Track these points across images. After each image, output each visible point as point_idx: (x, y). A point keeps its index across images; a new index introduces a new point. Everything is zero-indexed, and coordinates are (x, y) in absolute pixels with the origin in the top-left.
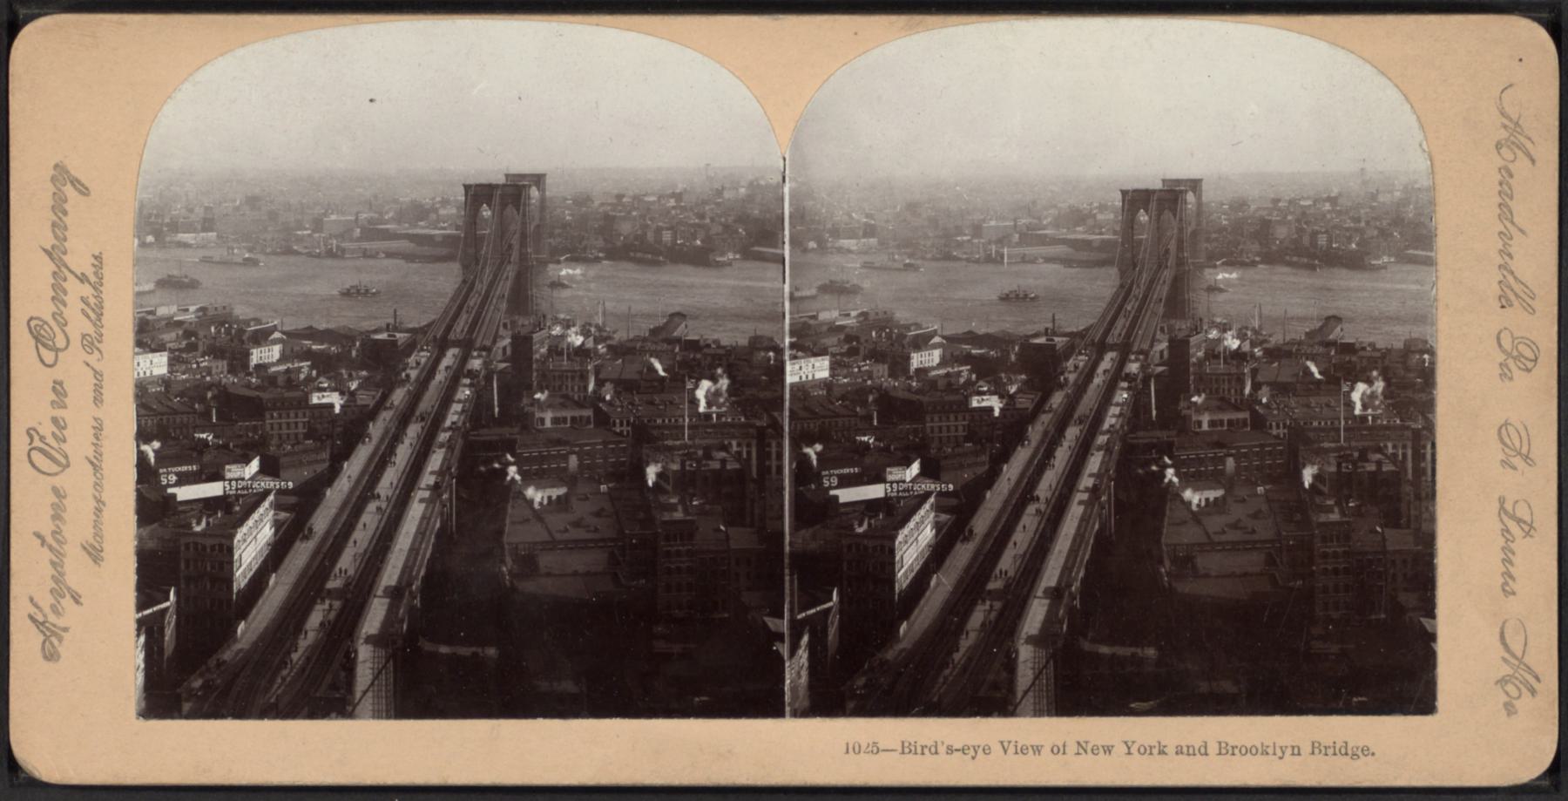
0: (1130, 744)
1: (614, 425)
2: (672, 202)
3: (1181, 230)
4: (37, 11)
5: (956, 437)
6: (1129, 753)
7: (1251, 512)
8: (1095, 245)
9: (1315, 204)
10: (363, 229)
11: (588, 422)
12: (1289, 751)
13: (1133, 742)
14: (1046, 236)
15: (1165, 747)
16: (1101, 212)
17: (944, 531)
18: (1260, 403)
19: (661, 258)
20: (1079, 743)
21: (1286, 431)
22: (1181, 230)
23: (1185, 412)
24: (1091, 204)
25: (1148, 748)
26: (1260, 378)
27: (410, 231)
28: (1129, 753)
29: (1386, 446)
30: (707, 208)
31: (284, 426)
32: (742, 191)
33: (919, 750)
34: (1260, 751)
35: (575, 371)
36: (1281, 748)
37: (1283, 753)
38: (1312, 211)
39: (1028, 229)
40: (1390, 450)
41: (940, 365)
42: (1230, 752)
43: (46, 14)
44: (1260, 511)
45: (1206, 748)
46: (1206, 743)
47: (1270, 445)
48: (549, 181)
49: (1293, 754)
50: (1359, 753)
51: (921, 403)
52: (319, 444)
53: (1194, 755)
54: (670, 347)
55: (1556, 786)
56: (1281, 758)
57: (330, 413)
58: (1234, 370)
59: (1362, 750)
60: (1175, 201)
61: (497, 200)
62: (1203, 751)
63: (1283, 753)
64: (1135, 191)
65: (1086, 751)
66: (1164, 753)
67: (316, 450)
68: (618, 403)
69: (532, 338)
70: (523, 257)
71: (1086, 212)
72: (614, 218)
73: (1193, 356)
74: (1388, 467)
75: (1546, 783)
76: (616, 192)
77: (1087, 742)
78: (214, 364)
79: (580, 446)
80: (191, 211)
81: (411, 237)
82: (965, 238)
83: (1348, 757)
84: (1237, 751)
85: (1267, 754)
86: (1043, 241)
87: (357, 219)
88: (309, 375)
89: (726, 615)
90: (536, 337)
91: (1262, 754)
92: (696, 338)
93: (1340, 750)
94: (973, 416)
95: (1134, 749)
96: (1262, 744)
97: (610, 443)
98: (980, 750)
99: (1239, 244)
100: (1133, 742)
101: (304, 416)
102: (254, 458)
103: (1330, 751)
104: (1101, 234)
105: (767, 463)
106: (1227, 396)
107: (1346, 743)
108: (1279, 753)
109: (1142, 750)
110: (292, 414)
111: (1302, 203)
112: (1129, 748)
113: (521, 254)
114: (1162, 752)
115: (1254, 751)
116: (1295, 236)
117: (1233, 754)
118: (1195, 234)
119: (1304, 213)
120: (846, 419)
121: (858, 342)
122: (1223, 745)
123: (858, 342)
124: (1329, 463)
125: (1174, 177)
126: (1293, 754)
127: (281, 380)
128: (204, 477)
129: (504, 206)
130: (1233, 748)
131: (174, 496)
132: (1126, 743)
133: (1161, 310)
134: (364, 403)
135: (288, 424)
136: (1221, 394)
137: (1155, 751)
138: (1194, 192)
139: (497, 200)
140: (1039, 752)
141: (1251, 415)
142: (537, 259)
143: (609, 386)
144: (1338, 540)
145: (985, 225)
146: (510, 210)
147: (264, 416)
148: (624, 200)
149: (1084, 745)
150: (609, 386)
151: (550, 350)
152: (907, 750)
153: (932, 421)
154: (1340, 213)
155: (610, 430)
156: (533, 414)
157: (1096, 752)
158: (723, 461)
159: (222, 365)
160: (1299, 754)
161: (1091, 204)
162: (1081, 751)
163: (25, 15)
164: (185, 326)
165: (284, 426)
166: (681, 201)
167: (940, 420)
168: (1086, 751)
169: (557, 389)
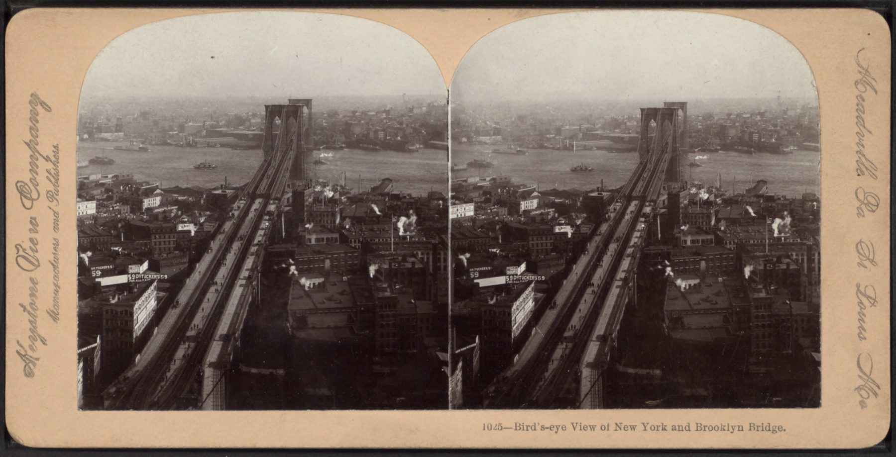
0: (646, 424)
2: (384, 115)
4: (21, 6)
5: (546, 249)
6: (645, 430)
9: (751, 117)
12: (736, 429)
13: (648, 423)
15: (666, 426)
18: (720, 230)
19: (378, 147)
20: (616, 424)
21: (735, 246)
23: (677, 235)
25: (656, 427)
26: (720, 216)
27: (235, 132)
28: (645, 430)
31: (162, 243)
32: (424, 109)
33: (525, 428)
34: (720, 429)
36: (732, 427)
37: (733, 430)
38: (750, 120)
42: (703, 429)
43: (26, 8)
45: (689, 427)
46: (689, 424)
47: (725, 254)
49: (739, 430)
50: (777, 429)
51: (526, 230)
52: (182, 253)
53: (683, 430)
55: (889, 449)
56: (732, 433)
59: (779, 428)
60: (672, 115)
61: (284, 114)
62: (687, 428)
63: (733, 430)
64: (648, 109)
65: (620, 429)
66: (665, 430)
68: (353, 230)
70: (299, 147)
71: (620, 121)
75: (883, 447)
76: (352, 109)
77: (621, 424)
79: (332, 254)
81: (235, 136)
83: (771, 432)
84: (707, 429)
85: (724, 430)
88: (177, 214)
91: (721, 430)
92: (398, 193)
93: (685, 428)
95: (648, 428)
96: (721, 424)
98: (560, 429)
99: (708, 139)
100: (648, 423)
102: (145, 261)
103: (760, 429)
105: (438, 264)
107: (769, 424)
108: (731, 430)
109: (653, 428)
112: (645, 427)
113: (298, 145)
114: (664, 429)
115: (716, 428)
116: (740, 135)
117: (705, 430)
118: (683, 133)
120: (105, 238)
122: (699, 425)
124: (759, 264)
126: (739, 430)
127: (160, 217)
129: (288, 118)
130: (705, 426)
131: (100, 283)
132: (643, 424)
135: (165, 242)
136: (698, 225)
137: (660, 429)
138: (683, 110)
139: (284, 114)
140: (594, 429)
142: (307, 148)
143: (348, 220)
146: (292, 120)
147: (151, 237)
149: (619, 425)
151: (314, 200)
152: (518, 428)
153: (533, 240)
155: (349, 245)
157: (626, 429)
159: (127, 208)
160: (742, 430)
161: (624, 116)
162: (618, 428)
163: (14, 8)
165: (162, 243)
167: (537, 240)
168: (620, 429)
169: (694, 223)
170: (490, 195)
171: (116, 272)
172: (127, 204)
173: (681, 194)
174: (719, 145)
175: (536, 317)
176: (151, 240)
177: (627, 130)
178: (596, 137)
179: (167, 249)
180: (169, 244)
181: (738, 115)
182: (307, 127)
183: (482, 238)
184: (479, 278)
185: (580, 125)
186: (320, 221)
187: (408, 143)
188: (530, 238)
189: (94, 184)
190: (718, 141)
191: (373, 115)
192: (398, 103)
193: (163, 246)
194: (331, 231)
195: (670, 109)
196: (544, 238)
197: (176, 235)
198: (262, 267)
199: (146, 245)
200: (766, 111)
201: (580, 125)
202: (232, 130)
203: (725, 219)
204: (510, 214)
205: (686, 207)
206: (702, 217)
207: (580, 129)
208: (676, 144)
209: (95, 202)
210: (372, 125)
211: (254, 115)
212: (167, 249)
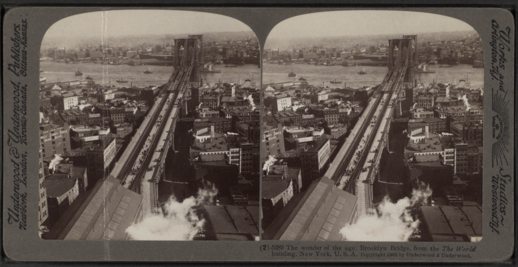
1: (441, 116)
2: (247, 43)
3: (195, 52)
8: (166, 58)
9: (242, 43)
11: (432, 115)
14: (148, 55)
16: (167, 46)
23: (411, 112)
27: (156, 55)
29: (480, 121)
30: (474, 44)
32: (423, 40)
35: (427, 100)
38: (242, 44)
40: (481, 123)
41: (328, 99)
44: (437, 142)
47: (218, 122)
48: (418, 37)
54: (460, 91)
58: (428, 98)
60: (193, 43)
61: (186, 44)
64: (179, 39)
65: (303, 255)
67: (128, 126)
68: (228, 109)
70: (409, 64)
71: (162, 47)
72: (441, 49)
74: (480, 128)
78: (93, 100)
79: (215, 123)
80: (82, 50)
81: (157, 58)
89: (477, 173)
94: (126, 115)
97: (440, 122)
101: (124, 115)
104: (168, 54)
110: (120, 115)
111: (238, 42)
115: (369, 249)
118: (414, 54)
128: (93, 134)
129: (402, 47)
136: (424, 106)
138: (414, 40)
139: (186, 44)
141: (220, 112)
142: (200, 64)
143: (439, 104)
144: (248, 150)
145: (127, 52)
147: (324, 116)
148: (230, 43)
150: (439, 104)
151: (205, 93)
153: (113, 116)
154: (250, 45)
155: (439, 118)
158: (477, 127)
161: (378, 45)
162: (302, 254)
164: (83, 88)
166: (465, 42)
167: (116, 116)
168: (303, 255)
170: (300, 92)
171: (93, 134)
172: (309, 99)
174: (436, 60)
176: (324, 118)
177: (165, 52)
178: (362, 58)
180: (121, 119)
182: (414, 51)
183: (298, 116)
188: (325, 116)
189: (289, 88)
191: (240, 43)
193: (331, 121)
197: (339, 115)
198: (175, 130)
199: (322, 121)
200: (466, 39)
201: (352, 51)
202: (369, 55)
204: (99, 102)
205: (203, 96)
207: (138, 52)
208: (196, 59)
209: (290, 98)
212: (334, 123)
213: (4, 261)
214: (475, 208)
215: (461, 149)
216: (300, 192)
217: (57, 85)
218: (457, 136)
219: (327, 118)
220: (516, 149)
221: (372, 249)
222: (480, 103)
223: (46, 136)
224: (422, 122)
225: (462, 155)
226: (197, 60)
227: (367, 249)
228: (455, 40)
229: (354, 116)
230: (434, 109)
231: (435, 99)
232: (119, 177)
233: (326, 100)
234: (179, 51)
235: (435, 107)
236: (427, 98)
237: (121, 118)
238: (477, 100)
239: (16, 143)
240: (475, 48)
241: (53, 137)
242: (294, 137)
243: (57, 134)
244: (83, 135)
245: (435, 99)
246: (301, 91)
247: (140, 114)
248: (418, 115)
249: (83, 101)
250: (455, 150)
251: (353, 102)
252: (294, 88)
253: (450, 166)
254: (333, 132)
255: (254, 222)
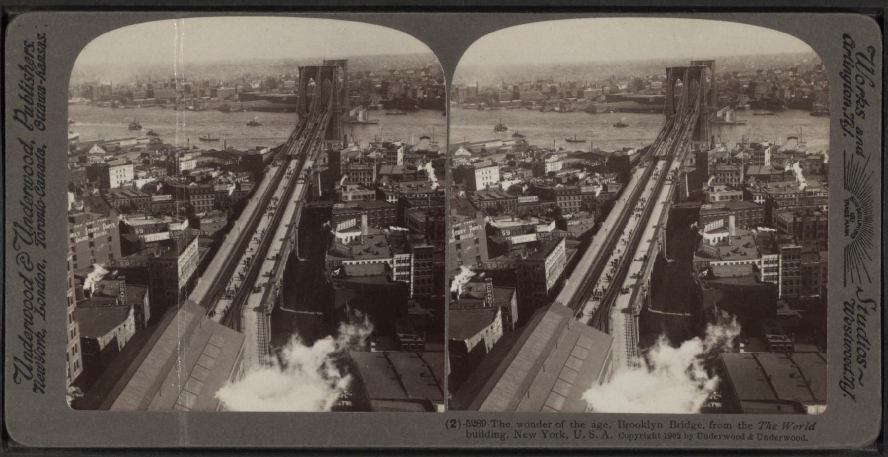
1: (755, 199)
2: (423, 73)
3: (335, 89)
7: (377, 243)
8: (284, 99)
10: (240, 95)
11: (741, 198)
16: (654, 81)
17: (204, 255)
18: (749, 186)
19: (416, 107)
22: (702, 90)
23: (705, 192)
24: (648, 77)
27: (268, 95)
29: (822, 208)
30: (812, 76)
32: (725, 68)
39: (244, 91)
41: (562, 170)
44: (382, 242)
47: (373, 209)
48: (717, 63)
50: (602, 426)
57: (593, 197)
60: (331, 73)
61: (319, 75)
64: (307, 67)
65: (520, 436)
68: (390, 187)
69: (707, 154)
70: (702, 109)
73: (710, 161)
74: (822, 219)
76: (757, 69)
79: (368, 210)
81: (269, 99)
82: (572, 99)
86: (620, 99)
87: (603, 91)
90: (710, 153)
94: (217, 196)
97: (386, 208)
99: (369, 97)
101: (212, 197)
104: (288, 93)
106: (730, 183)
113: (333, 106)
115: (632, 425)
116: (404, 91)
119: (776, 78)
121: (514, 158)
123: (514, 158)
125: (697, 60)
128: (159, 230)
129: (690, 80)
133: (690, 136)
134: (245, 189)
138: (710, 68)
139: (319, 75)
143: (752, 179)
145: (585, 91)
146: (327, 81)
147: (556, 199)
148: (395, 73)
153: (194, 198)
155: (753, 202)
156: (709, 194)
158: (818, 217)
161: (648, 77)
164: (142, 151)
167: (199, 198)
171: (525, 232)
173: (342, 151)
174: (748, 103)
175: (568, 271)
179: (573, 210)
180: (208, 203)
181: (401, 71)
182: (710, 87)
184: (510, 236)
185: (236, 86)
186: (724, 180)
187: (815, 101)
188: (558, 199)
190: (748, 99)
192: (805, 61)
194: (369, 188)
195: (697, 68)
196: (572, 198)
199: (551, 207)
203: (387, 175)
206: (364, 174)
210: (410, 84)
211: (655, 79)
212: (573, 210)
213: (7, 447)
214: (815, 355)
215: (790, 256)
216: (148, 327)
217: (98, 145)
218: (784, 233)
219: (560, 202)
220: (884, 255)
221: (638, 426)
222: (823, 177)
223: (79, 233)
224: (723, 209)
225: (792, 265)
226: (706, 104)
227: (628, 426)
228: (781, 69)
229: (607, 199)
230: (744, 187)
231: (746, 170)
232: (204, 303)
233: (558, 172)
234: (306, 88)
235: (746, 183)
236: (732, 167)
237: (208, 201)
238: (818, 172)
239: (28, 246)
240: (815, 83)
241: (91, 235)
242: (504, 234)
243: (98, 229)
244: (142, 231)
245: (746, 170)
246: (517, 156)
247: (239, 195)
248: (717, 197)
249: (143, 174)
250: (781, 257)
251: (606, 175)
252: (504, 151)
253: (772, 283)
254: (204, 224)
255: (436, 380)
